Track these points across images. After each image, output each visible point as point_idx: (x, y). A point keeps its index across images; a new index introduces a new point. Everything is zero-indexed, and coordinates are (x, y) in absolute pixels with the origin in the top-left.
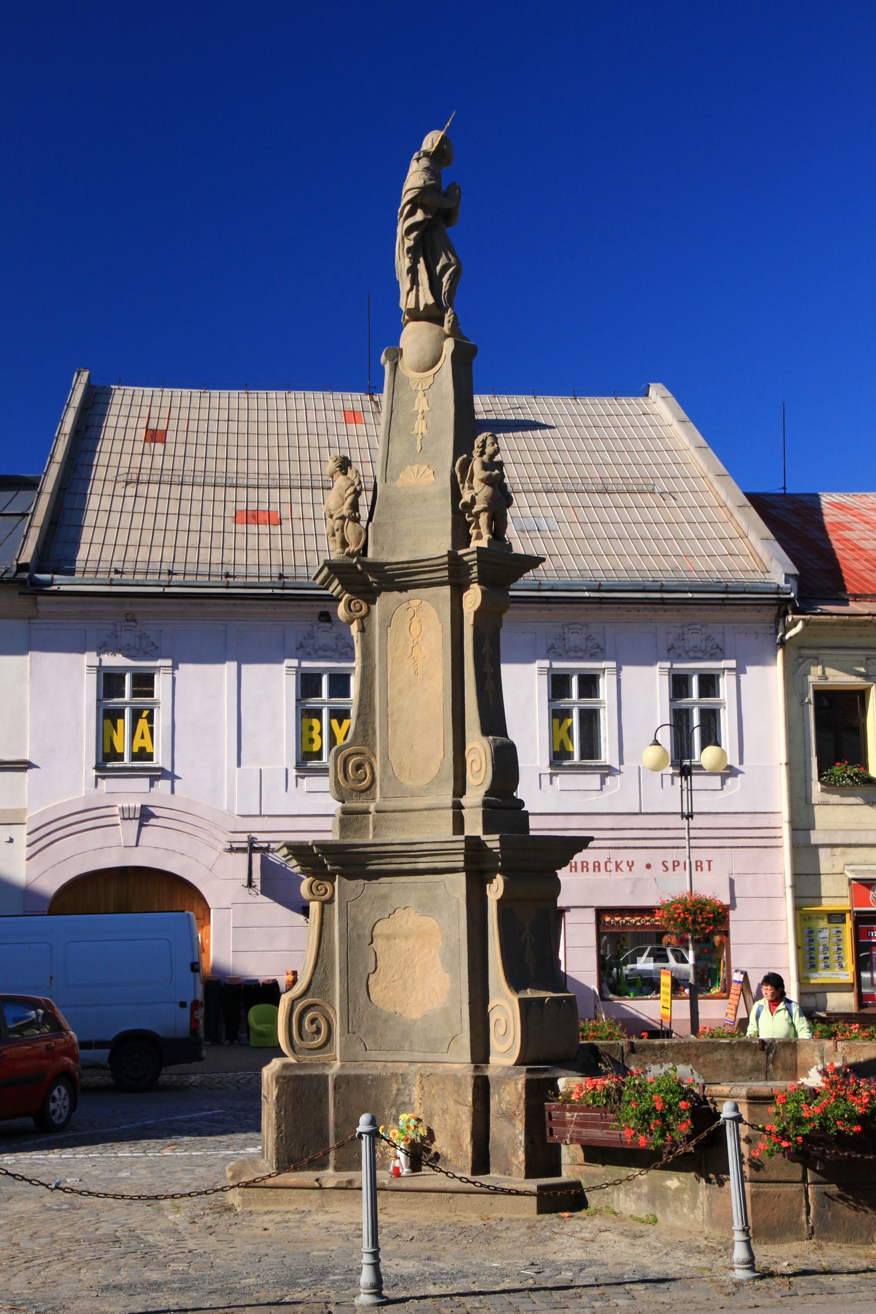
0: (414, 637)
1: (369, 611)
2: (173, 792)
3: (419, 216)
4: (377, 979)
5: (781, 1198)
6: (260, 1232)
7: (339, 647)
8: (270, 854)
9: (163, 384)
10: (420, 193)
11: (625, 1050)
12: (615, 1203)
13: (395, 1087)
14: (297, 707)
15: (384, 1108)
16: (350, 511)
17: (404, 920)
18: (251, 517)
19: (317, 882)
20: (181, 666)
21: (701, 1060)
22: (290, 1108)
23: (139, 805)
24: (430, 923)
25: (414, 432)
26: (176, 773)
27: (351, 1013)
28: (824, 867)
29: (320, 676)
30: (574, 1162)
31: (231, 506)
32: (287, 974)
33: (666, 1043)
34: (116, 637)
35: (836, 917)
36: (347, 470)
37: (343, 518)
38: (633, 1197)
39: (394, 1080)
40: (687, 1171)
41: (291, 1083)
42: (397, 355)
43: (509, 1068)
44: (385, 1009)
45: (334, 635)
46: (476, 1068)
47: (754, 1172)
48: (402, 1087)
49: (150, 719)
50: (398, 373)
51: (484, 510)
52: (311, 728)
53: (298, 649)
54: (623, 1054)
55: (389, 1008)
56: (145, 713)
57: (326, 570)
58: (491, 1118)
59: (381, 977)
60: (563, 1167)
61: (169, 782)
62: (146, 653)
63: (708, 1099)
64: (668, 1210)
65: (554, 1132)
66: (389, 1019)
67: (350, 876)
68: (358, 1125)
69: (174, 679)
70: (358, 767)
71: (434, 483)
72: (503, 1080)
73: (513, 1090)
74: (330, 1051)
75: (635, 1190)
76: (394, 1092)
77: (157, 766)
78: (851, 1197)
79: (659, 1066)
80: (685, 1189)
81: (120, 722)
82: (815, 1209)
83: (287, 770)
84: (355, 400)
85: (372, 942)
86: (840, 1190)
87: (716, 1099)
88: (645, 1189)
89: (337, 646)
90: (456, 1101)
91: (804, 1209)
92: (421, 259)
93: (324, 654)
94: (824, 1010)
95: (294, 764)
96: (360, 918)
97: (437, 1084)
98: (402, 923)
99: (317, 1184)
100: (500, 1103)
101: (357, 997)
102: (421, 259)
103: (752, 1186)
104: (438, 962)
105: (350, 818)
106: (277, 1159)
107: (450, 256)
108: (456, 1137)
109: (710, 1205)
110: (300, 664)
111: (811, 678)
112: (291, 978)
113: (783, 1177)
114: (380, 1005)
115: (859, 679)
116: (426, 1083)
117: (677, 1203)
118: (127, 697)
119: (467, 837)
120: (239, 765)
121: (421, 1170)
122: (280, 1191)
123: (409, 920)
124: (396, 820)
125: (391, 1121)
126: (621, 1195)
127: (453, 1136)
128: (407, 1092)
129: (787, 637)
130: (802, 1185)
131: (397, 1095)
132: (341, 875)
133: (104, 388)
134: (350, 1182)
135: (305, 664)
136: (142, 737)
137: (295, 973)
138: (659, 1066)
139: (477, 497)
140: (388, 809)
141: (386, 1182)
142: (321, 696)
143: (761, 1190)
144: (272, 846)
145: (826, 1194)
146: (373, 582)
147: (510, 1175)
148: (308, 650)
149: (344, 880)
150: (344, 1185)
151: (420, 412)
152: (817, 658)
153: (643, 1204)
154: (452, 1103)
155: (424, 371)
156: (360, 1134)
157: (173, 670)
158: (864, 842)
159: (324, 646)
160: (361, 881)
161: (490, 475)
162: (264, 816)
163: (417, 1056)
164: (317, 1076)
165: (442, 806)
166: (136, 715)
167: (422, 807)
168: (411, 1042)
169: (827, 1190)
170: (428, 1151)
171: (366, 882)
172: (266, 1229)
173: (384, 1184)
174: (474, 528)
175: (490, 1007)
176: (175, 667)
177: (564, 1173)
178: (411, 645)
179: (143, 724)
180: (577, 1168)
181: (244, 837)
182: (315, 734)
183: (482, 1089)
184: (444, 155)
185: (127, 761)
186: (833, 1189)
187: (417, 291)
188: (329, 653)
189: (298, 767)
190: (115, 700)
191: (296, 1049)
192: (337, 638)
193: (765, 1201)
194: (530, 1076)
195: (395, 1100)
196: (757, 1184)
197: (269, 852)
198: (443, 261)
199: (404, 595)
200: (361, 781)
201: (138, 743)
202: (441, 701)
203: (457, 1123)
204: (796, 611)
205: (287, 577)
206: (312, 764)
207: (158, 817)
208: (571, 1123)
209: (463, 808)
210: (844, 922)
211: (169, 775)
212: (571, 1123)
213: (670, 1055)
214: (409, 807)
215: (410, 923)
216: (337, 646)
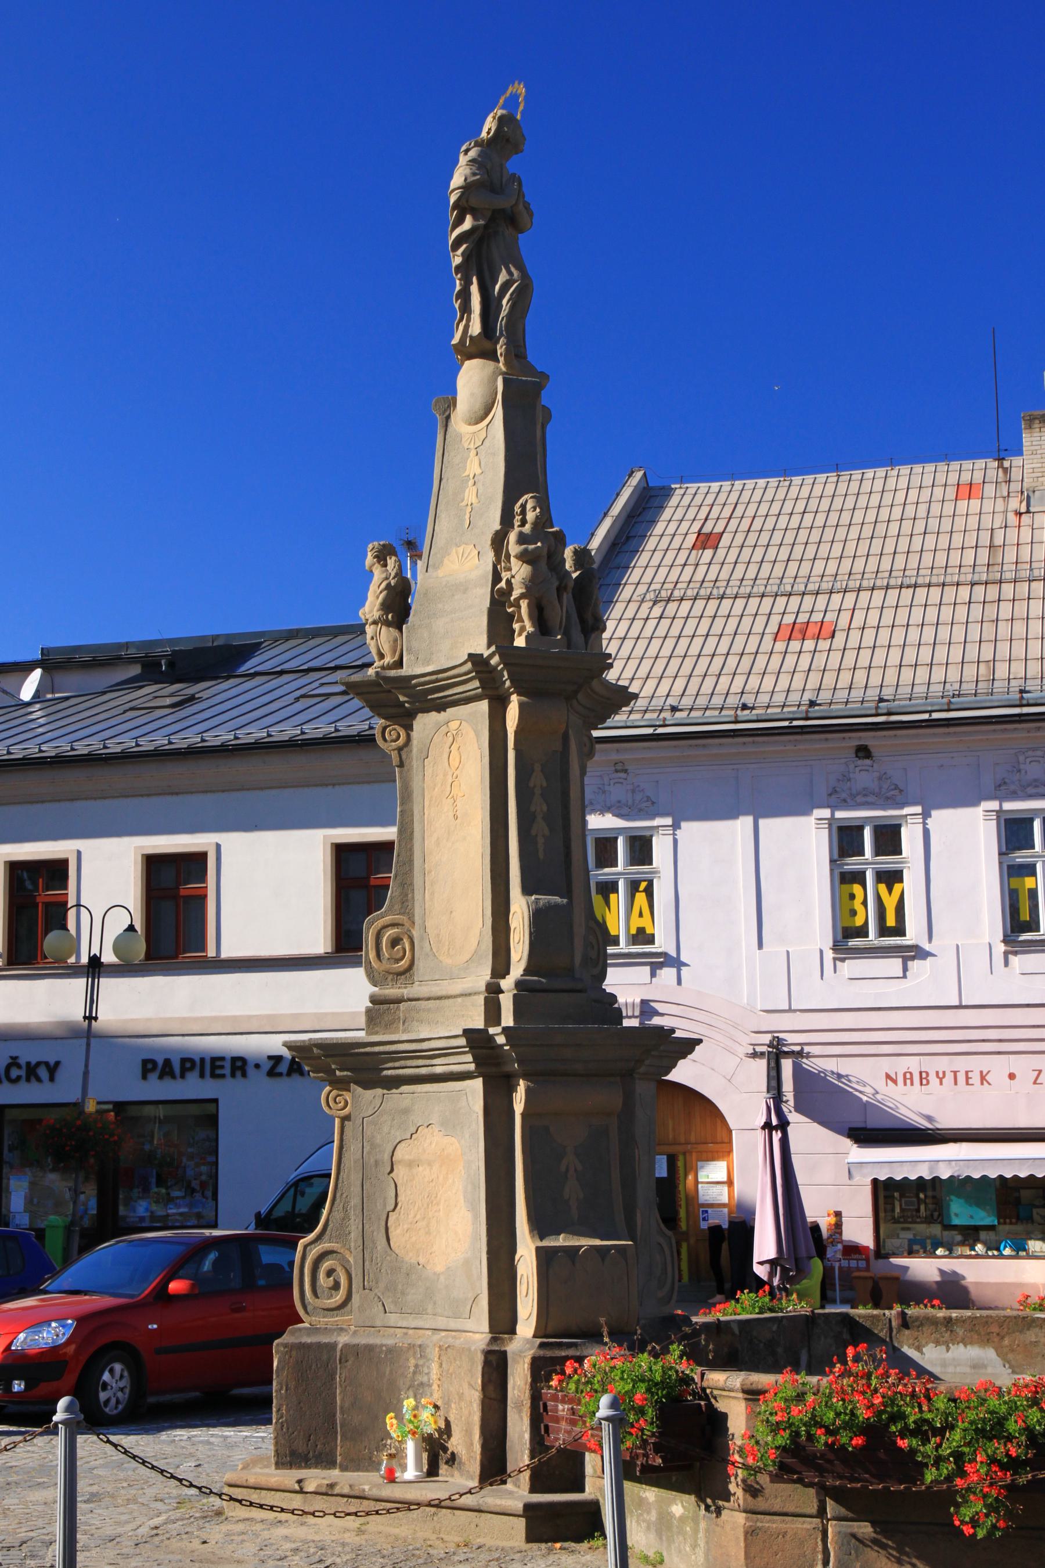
0: (453, 769)
1: (409, 738)
2: (679, 982)
3: (468, 224)
4: (398, 1219)
5: (788, 1537)
6: (196, 1544)
7: (884, 791)
8: (804, 1060)
9: (733, 477)
10: (462, 194)
11: (894, 1324)
14: (832, 870)
15: (400, 1390)
16: (380, 613)
17: (428, 1141)
18: (798, 631)
19: (334, 1093)
20: (683, 824)
21: (1006, 1342)
22: (292, 1385)
23: (638, 1001)
25: (464, 504)
26: (683, 958)
27: (367, 1263)
29: (860, 829)
31: (775, 620)
32: (829, 1215)
33: (954, 1315)
34: (604, 792)
36: (386, 560)
38: (644, 1525)
39: (411, 1352)
40: (689, 1494)
41: (294, 1353)
42: (449, 407)
44: (407, 1259)
45: (876, 774)
46: (494, 1340)
47: (750, 1499)
48: (421, 1362)
49: (649, 892)
50: (450, 429)
51: (522, 596)
52: (852, 897)
53: (830, 795)
54: (891, 1329)
55: (410, 1258)
56: (643, 885)
58: (509, 1408)
60: (587, 1479)
61: (675, 970)
62: (640, 810)
63: (708, 1391)
65: (550, 1430)
66: (411, 1272)
67: (367, 1085)
68: (55, 1412)
69: (675, 841)
70: (395, 942)
71: (477, 567)
72: (519, 1354)
76: (412, 1369)
77: (659, 950)
78: (890, 1543)
79: (944, 1347)
81: (613, 897)
82: (836, 1556)
83: (821, 952)
84: (976, 469)
85: (392, 1170)
86: (875, 1532)
87: (715, 1392)
89: (881, 788)
91: (820, 1556)
92: (475, 279)
93: (864, 799)
95: (831, 944)
96: (378, 1141)
99: (297, 1487)
101: (374, 1242)
102: (475, 279)
103: (747, 1519)
105: (381, 1010)
106: (276, 1451)
107: (513, 269)
108: (468, 1433)
109: (707, 1543)
110: (833, 814)
112: (833, 1220)
113: (791, 1509)
114: (400, 1252)
116: (444, 1358)
118: (620, 867)
119: (504, 1029)
120: (760, 945)
121: (437, 1475)
122: (264, 1492)
123: (433, 1142)
124: (429, 1010)
128: (426, 1370)
130: (819, 1520)
131: (414, 1373)
132: (358, 1083)
133: (663, 488)
134: (332, 1486)
135: (839, 814)
136: (641, 915)
137: (838, 1214)
138: (944, 1347)
139: (513, 580)
140: (421, 996)
141: (367, 1488)
142: (863, 855)
143: (759, 1524)
144: (807, 1049)
145: (854, 1536)
148: (844, 795)
150: (324, 1490)
151: (471, 476)
156: (56, 1424)
157: (674, 830)
159: (864, 789)
160: (379, 1091)
161: (526, 550)
162: (795, 1011)
163: (441, 1322)
164: (327, 1345)
166: (634, 886)
167: (458, 992)
168: (435, 1303)
169: (856, 1530)
170: (445, 1449)
171: (385, 1091)
172: (205, 1542)
173: (364, 1490)
174: (517, 622)
175: (517, 1257)
176: (676, 826)
177: (588, 1488)
178: (450, 781)
179: (641, 898)
181: (767, 1038)
182: (857, 904)
183: (495, 1367)
184: (508, 140)
185: (623, 947)
186: (865, 1529)
187: (469, 320)
188: (870, 799)
189: (836, 947)
190: (607, 870)
191: (309, 1308)
192: (880, 778)
193: (764, 1541)
194: (541, 1353)
195: (413, 1380)
196: (754, 1516)
197: (803, 1057)
198: (503, 277)
199: (443, 716)
200: (398, 961)
201: (636, 923)
202: (480, 851)
205: (820, 705)
206: (854, 942)
207: (662, 1015)
209: (502, 992)
211: (675, 962)
213: (960, 1332)
215: (433, 1146)
216: (881, 788)
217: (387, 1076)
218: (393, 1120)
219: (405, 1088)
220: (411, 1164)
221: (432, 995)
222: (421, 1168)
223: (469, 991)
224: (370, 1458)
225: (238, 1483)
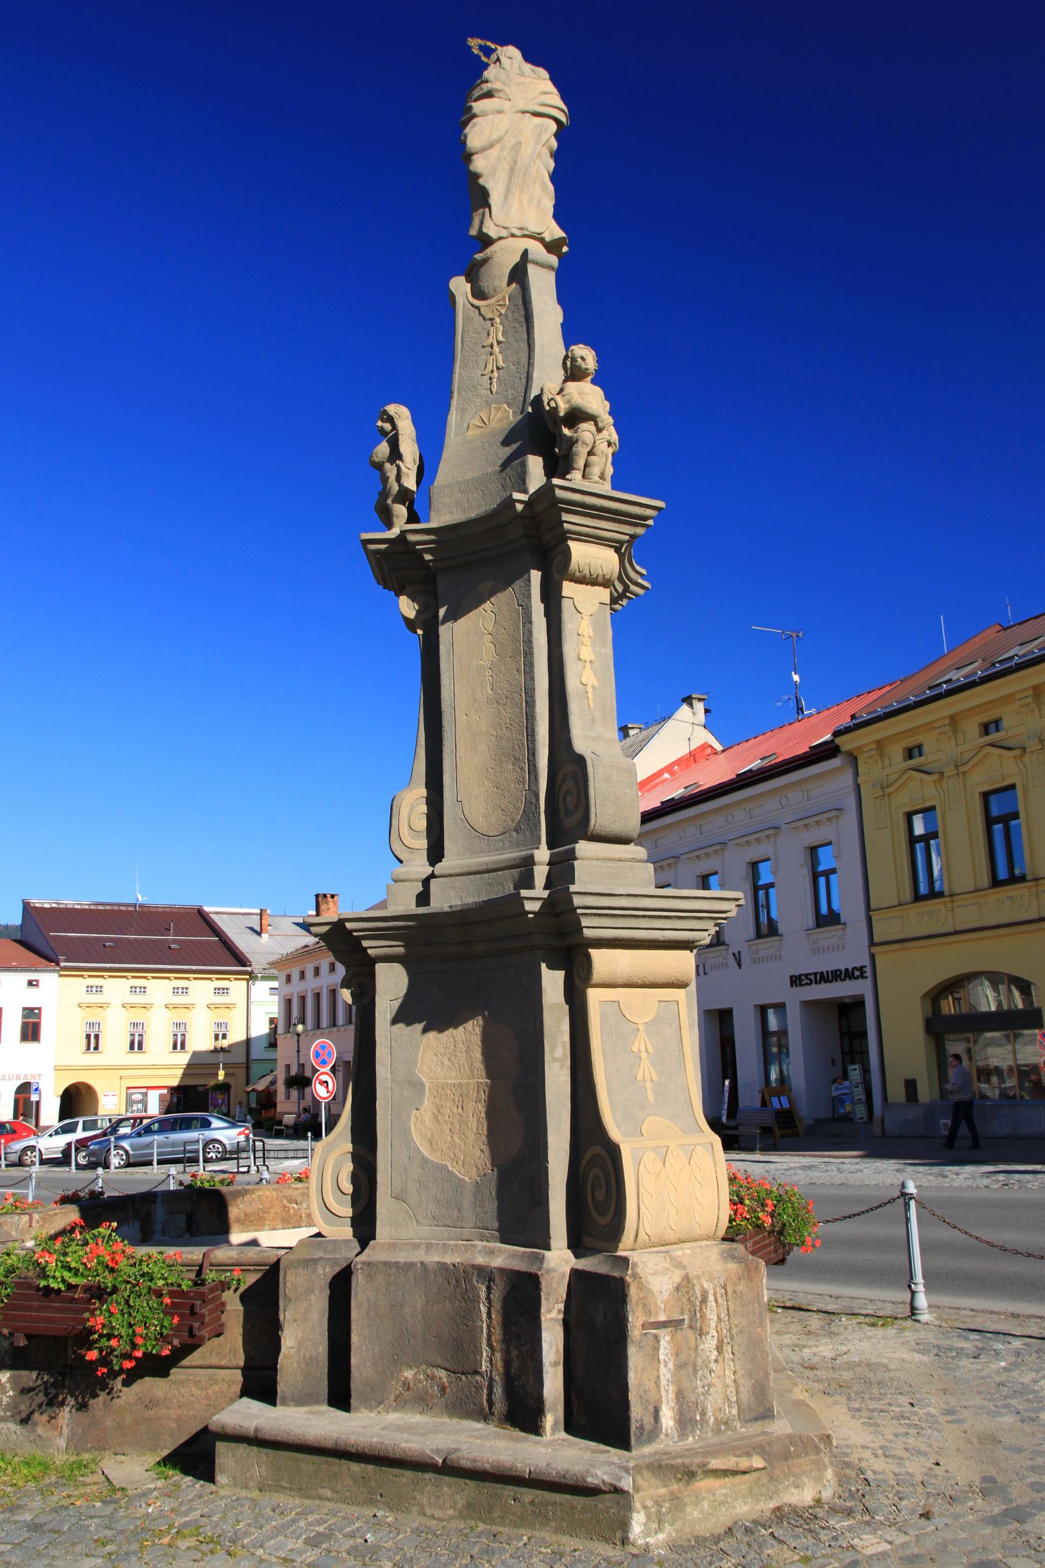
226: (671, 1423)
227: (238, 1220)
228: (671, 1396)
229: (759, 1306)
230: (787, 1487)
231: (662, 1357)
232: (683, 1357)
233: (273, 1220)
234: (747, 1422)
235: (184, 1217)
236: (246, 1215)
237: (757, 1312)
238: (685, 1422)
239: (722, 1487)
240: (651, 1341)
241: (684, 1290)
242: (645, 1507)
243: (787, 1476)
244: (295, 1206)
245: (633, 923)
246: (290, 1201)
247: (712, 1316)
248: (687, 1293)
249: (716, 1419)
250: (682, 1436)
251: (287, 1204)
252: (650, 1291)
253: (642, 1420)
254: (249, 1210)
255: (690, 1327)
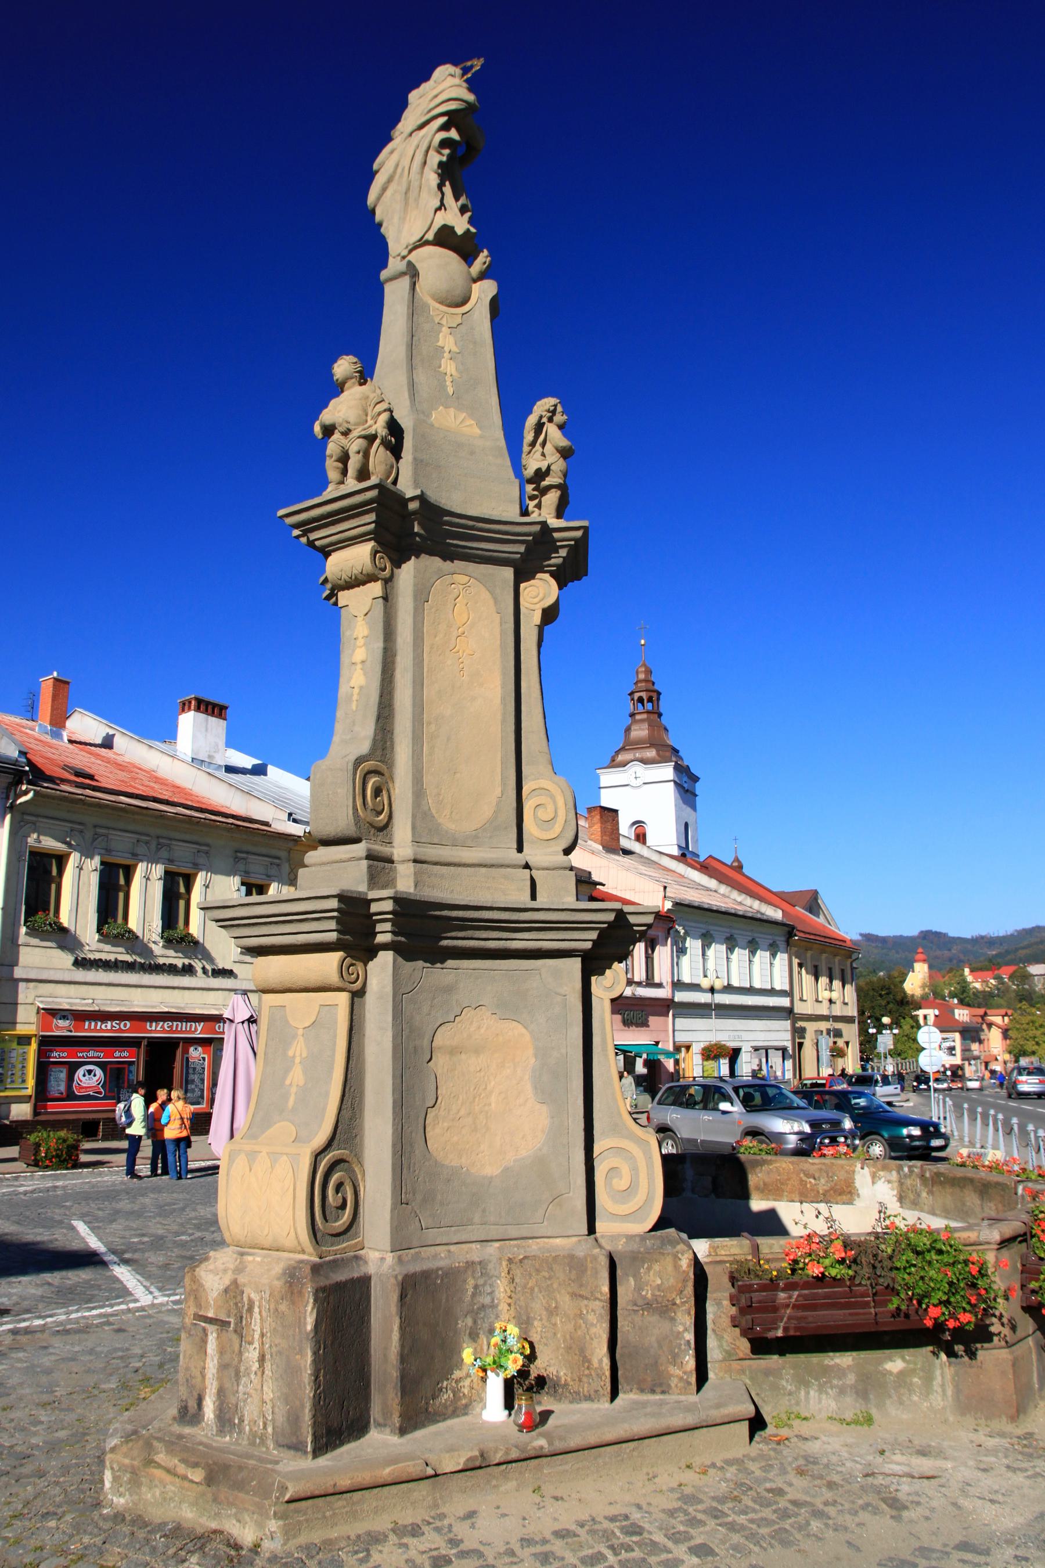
4: (436, 1116)
12: (802, 1404)
13: (471, 1282)
24: (515, 1030)
27: (405, 1171)
28: (21, 998)
30: (729, 1356)
35: (24, 1040)
37: (371, 439)
43: (642, 1238)
44: (446, 1163)
48: (481, 1282)
55: (451, 1160)
57: (374, 493)
59: (442, 1113)
64: (888, 1402)
73: (670, 1268)
74: (356, 1235)
75: (835, 1382)
76: (470, 1291)
80: (913, 1371)
88: (851, 1379)
90: (574, 1295)
94: (7, 1118)
97: (538, 1271)
98: (472, 1029)
100: (639, 1289)
101: (411, 1145)
104: (528, 1087)
111: (29, 840)
115: (64, 846)
116: (517, 1272)
117: (902, 1391)
124: (442, 876)
125: (466, 1338)
126: (812, 1393)
127: (569, 1348)
129: (19, 802)
131: (474, 1295)
146: (417, 534)
147: (663, 1392)
149: (400, 959)
152: (34, 823)
153: (849, 1399)
154: (567, 1298)
155: (450, 306)
158: (52, 978)
163: (494, 1232)
165: (506, 862)
168: (484, 1211)
180: (736, 1365)
195: (472, 1304)
199: (448, 565)
203: (576, 1328)
204: (30, 783)
208: (787, 1306)
210: (29, 1044)
212: (787, 1306)
214: (456, 860)
215: (482, 1031)
217: (442, 947)
218: (434, 998)
219: (450, 963)
220: (454, 1051)
221: (442, 860)
222: (463, 1056)
223: (493, 862)
224: (427, 1410)
225: (317, 1493)
226: (212, 1416)
227: (757, 1188)
228: (214, 1391)
229: (300, 1332)
230: (229, 1516)
231: (209, 1351)
232: (227, 1358)
233: (790, 1193)
234: (280, 1446)
235: (710, 1179)
236: (765, 1184)
237: (297, 1338)
238: (226, 1419)
239: (171, 1483)
240: (201, 1334)
241: (232, 1294)
242: (112, 1468)
243: (231, 1504)
244: (813, 1181)
245: (265, 930)
246: (808, 1175)
247: (256, 1326)
248: (235, 1297)
249: (251, 1430)
250: (221, 1431)
251: (804, 1178)
252: (201, 1285)
253: (186, 1401)
254: (767, 1180)
255: (235, 1331)
